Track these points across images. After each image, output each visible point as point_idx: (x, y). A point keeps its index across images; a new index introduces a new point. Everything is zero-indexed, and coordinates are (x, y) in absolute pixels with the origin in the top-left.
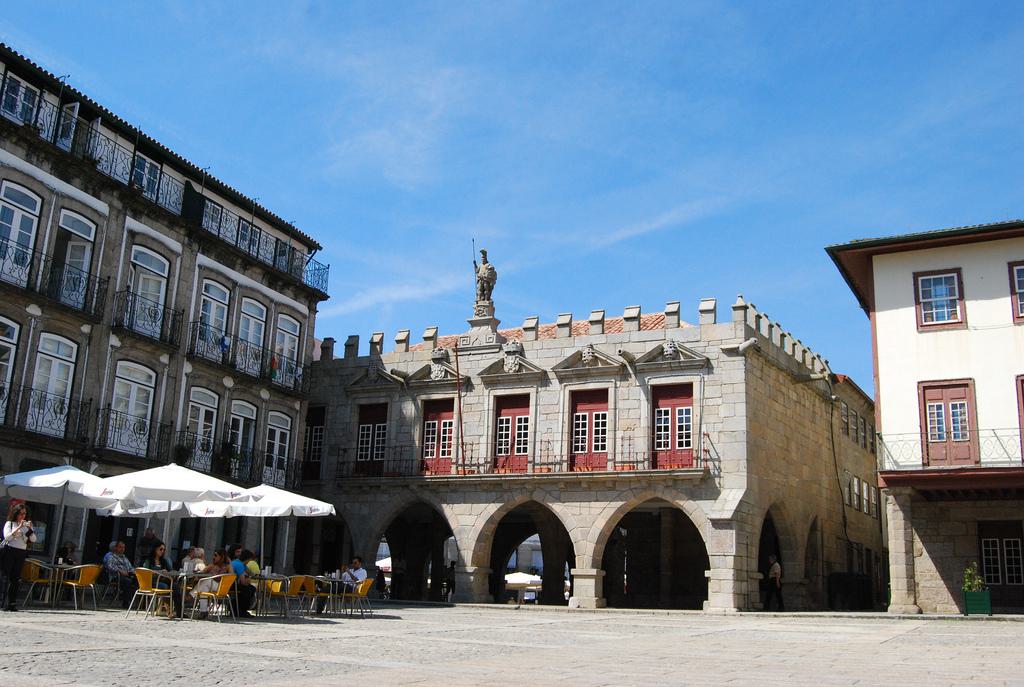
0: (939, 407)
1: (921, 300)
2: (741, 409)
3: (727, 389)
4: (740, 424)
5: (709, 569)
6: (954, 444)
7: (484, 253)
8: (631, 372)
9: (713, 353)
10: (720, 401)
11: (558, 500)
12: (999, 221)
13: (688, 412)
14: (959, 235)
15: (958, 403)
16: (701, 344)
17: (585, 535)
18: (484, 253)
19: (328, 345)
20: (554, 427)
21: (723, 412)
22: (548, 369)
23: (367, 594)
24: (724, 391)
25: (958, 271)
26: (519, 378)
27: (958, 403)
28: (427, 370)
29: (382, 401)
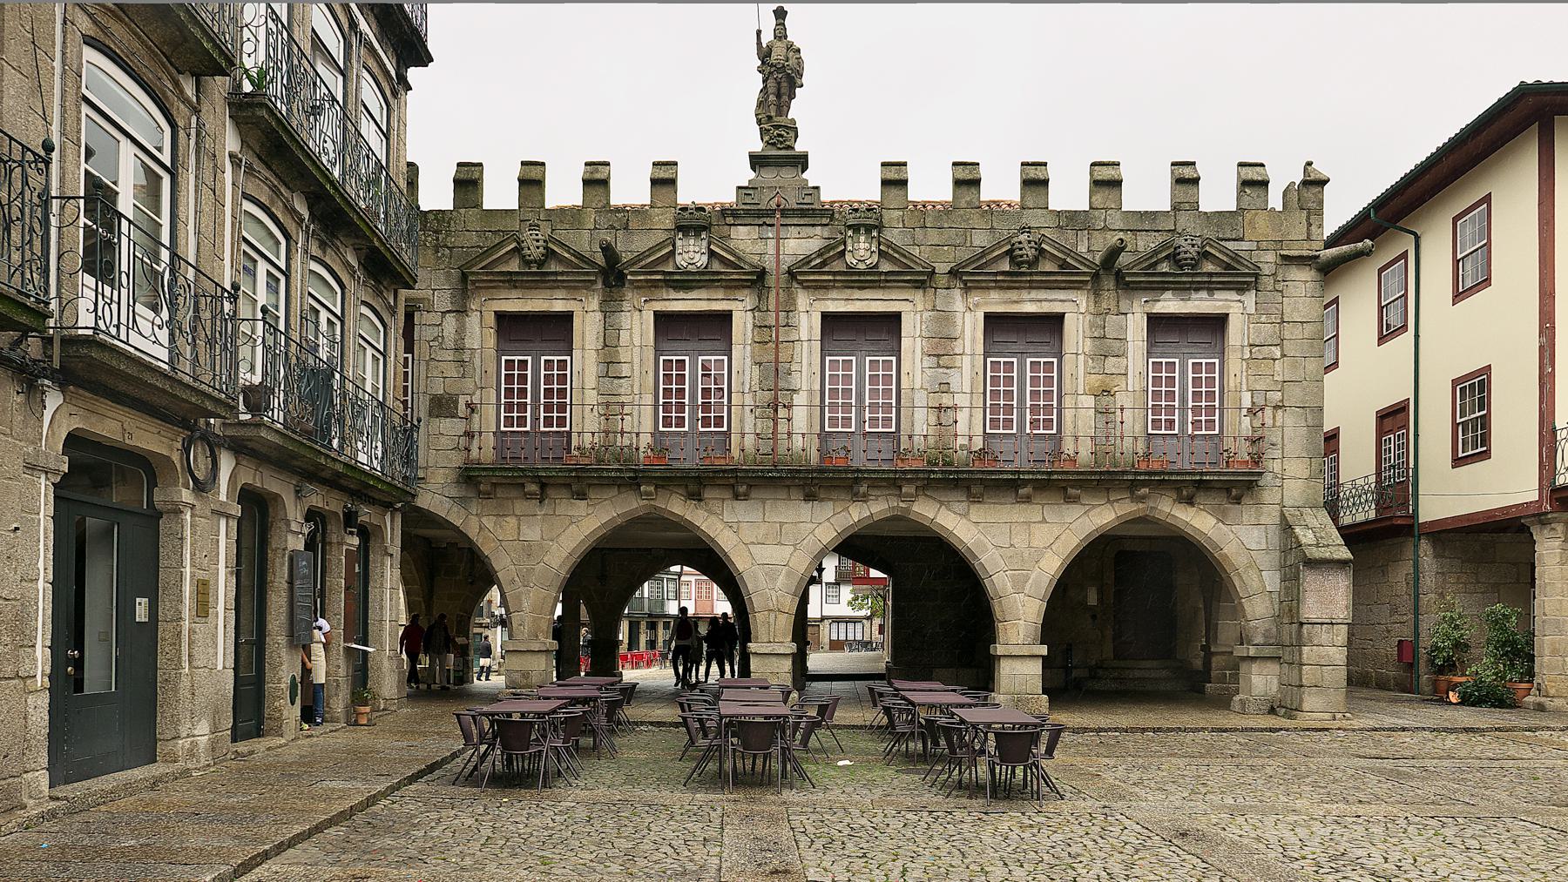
13: (562, 365)
17: (1019, 586)
19: (468, 181)
29: (558, 304)
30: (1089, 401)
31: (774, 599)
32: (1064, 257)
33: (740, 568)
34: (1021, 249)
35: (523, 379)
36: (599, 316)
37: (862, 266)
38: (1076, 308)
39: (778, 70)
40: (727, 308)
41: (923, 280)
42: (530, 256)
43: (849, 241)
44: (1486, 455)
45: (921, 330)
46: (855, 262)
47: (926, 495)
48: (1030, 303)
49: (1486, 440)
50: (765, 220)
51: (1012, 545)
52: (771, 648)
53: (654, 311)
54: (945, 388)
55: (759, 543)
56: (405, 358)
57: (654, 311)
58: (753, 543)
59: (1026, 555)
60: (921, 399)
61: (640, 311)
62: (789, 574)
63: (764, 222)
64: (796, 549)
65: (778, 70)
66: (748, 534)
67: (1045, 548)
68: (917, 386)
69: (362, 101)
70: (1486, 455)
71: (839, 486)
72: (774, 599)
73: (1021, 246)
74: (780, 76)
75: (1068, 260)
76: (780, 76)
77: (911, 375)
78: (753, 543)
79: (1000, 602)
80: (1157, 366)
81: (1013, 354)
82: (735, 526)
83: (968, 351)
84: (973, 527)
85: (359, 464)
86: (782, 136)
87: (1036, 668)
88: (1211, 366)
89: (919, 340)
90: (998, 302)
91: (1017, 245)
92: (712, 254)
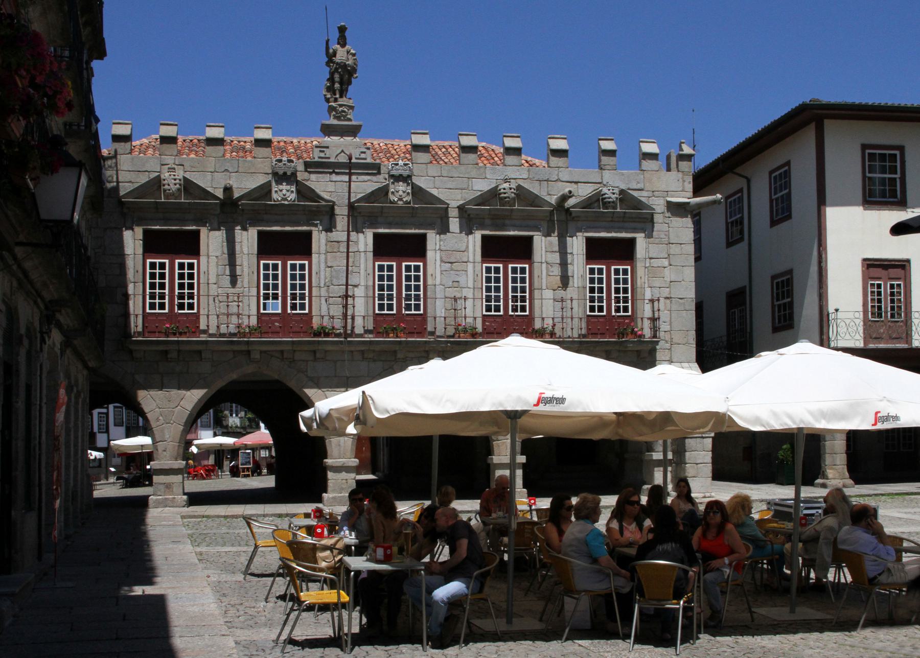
0: (879, 286)
1: (774, 197)
2: (689, 274)
3: (674, 249)
4: (688, 291)
5: (326, 493)
6: (870, 323)
7: (342, 30)
8: (194, 228)
9: (658, 205)
10: (666, 263)
11: (205, 394)
12: (877, 102)
14: (828, 109)
15: (895, 283)
16: (644, 194)
18: (342, 30)
20: (462, 280)
21: (669, 274)
22: (454, 204)
23: (807, 434)
24: (672, 252)
25: (901, 149)
26: (407, 215)
27: (895, 283)
28: (264, 191)
34: (505, 193)
46: (396, 199)
89: (438, 252)
91: (502, 191)
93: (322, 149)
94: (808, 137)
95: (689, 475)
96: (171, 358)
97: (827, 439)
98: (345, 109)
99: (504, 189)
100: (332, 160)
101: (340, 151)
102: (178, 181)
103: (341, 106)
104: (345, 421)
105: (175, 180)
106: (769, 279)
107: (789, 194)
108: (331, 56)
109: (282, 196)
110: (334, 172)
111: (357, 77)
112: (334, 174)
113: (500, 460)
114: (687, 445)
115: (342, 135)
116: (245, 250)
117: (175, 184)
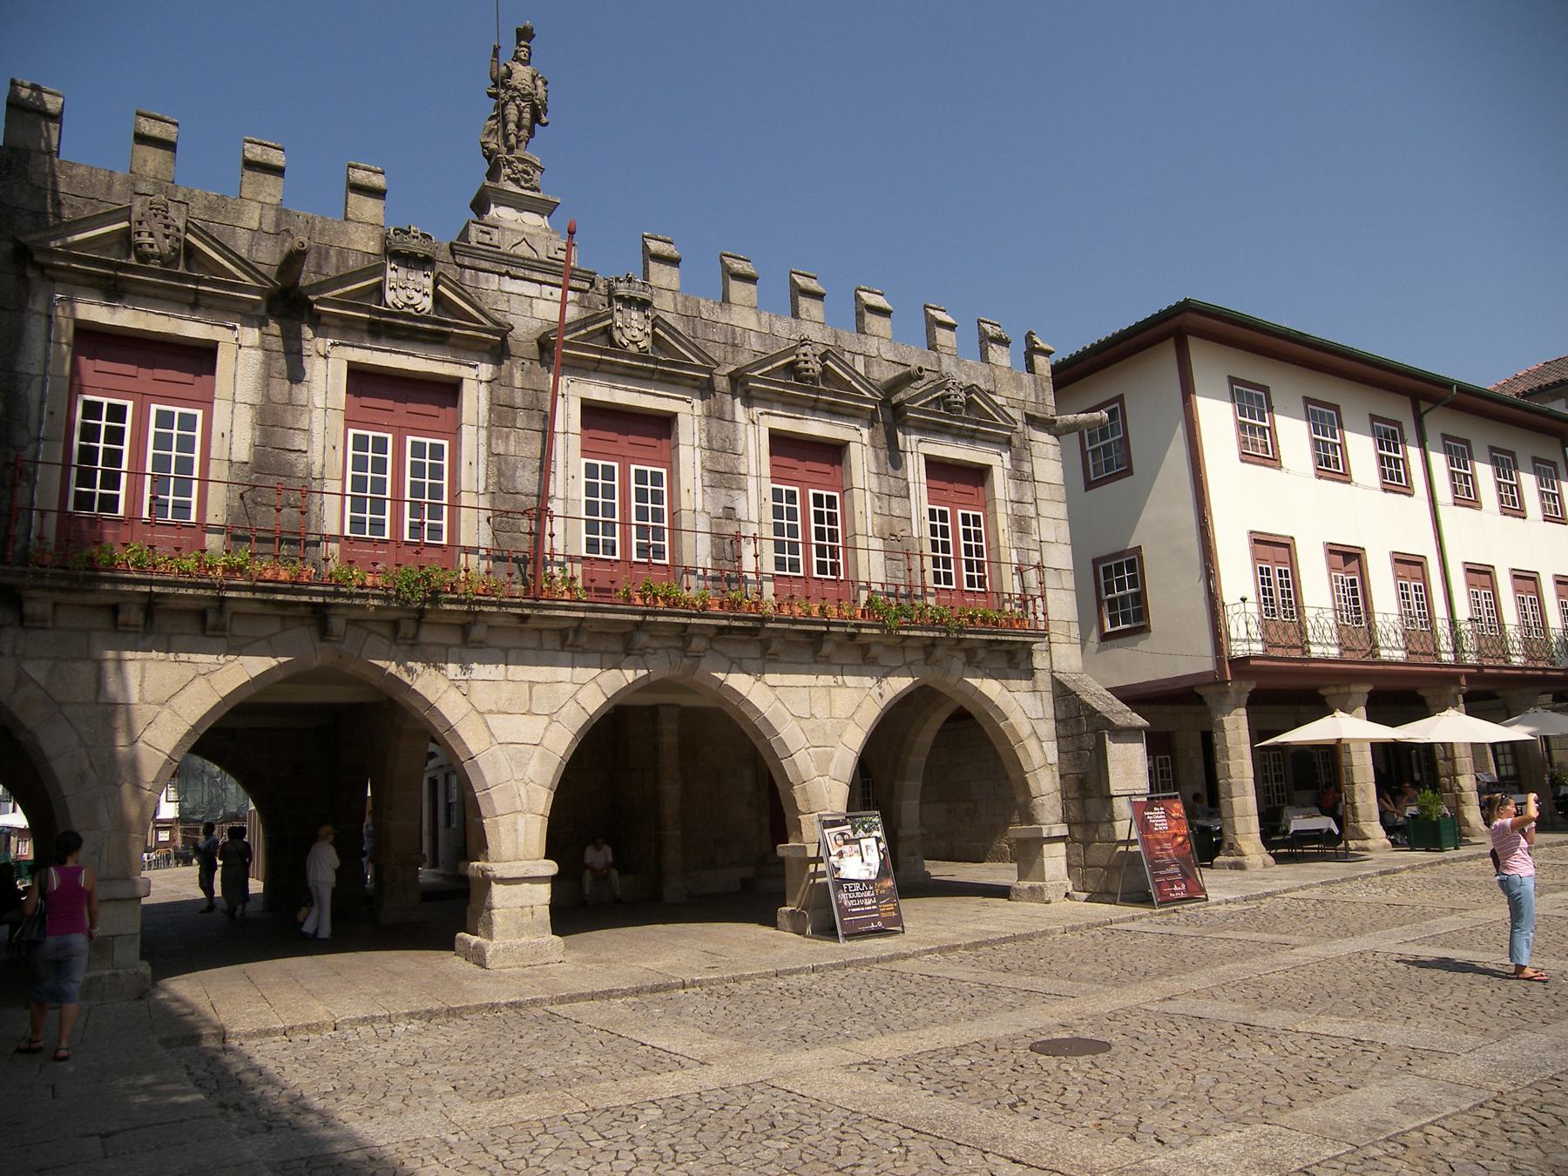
1: (1088, 448)
7: (524, 35)
17: (823, 765)
30: (877, 544)
31: (523, 793)
32: (849, 379)
33: (473, 746)
34: (806, 362)
35: (380, 466)
36: (258, 355)
37: (633, 349)
38: (689, 414)
39: (523, 97)
40: (840, 436)
41: (497, 348)
42: (151, 246)
43: (617, 316)
44: (1143, 630)
45: (700, 439)
46: (625, 342)
47: (715, 650)
48: (816, 427)
49: (1142, 613)
50: (509, 268)
51: (812, 715)
52: (524, 869)
53: (348, 362)
54: (730, 513)
55: (499, 712)
56: (930, 510)
57: (348, 362)
58: (490, 712)
59: (828, 728)
60: (703, 524)
61: (326, 357)
62: (544, 758)
63: (507, 272)
64: (552, 721)
65: (523, 97)
66: (484, 696)
67: (847, 719)
68: (699, 508)
69: (1525, 395)
70: (1143, 630)
71: (607, 634)
72: (523, 793)
73: (807, 358)
74: (523, 104)
75: (853, 383)
76: (523, 104)
77: (692, 492)
78: (490, 712)
79: (804, 789)
80: (360, 442)
81: (612, 457)
82: (464, 684)
83: (753, 471)
84: (768, 691)
85: (1486, 671)
86: (528, 174)
87: (544, 892)
88: (437, 451)
89: (698, 450)
90: (601, 392)
91: (802, 357)
92: (438, 299)
93: (486, 229)
94: (1164, 364)
95: (497, 869)
96: (126, 625)
97: (1234, 794)
98: (529, 169)
99: (805, 355)
100: (505, 248)
101: (520, 238)
102: (171, 231)
103: (521, 160)
104: (458, 779)
105: (167, 227)
106: (1090, 566)
107: (1125, 440)
108: (501, 81)
109: (406, 300)
110: (507, 274)
111: (546, 124)
112: (507, 278)
113: (1244, 815)
114: (1115, 804)
115: (521, 209)
116: (319, 401)
117: (167, 236)
